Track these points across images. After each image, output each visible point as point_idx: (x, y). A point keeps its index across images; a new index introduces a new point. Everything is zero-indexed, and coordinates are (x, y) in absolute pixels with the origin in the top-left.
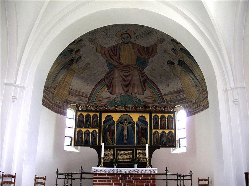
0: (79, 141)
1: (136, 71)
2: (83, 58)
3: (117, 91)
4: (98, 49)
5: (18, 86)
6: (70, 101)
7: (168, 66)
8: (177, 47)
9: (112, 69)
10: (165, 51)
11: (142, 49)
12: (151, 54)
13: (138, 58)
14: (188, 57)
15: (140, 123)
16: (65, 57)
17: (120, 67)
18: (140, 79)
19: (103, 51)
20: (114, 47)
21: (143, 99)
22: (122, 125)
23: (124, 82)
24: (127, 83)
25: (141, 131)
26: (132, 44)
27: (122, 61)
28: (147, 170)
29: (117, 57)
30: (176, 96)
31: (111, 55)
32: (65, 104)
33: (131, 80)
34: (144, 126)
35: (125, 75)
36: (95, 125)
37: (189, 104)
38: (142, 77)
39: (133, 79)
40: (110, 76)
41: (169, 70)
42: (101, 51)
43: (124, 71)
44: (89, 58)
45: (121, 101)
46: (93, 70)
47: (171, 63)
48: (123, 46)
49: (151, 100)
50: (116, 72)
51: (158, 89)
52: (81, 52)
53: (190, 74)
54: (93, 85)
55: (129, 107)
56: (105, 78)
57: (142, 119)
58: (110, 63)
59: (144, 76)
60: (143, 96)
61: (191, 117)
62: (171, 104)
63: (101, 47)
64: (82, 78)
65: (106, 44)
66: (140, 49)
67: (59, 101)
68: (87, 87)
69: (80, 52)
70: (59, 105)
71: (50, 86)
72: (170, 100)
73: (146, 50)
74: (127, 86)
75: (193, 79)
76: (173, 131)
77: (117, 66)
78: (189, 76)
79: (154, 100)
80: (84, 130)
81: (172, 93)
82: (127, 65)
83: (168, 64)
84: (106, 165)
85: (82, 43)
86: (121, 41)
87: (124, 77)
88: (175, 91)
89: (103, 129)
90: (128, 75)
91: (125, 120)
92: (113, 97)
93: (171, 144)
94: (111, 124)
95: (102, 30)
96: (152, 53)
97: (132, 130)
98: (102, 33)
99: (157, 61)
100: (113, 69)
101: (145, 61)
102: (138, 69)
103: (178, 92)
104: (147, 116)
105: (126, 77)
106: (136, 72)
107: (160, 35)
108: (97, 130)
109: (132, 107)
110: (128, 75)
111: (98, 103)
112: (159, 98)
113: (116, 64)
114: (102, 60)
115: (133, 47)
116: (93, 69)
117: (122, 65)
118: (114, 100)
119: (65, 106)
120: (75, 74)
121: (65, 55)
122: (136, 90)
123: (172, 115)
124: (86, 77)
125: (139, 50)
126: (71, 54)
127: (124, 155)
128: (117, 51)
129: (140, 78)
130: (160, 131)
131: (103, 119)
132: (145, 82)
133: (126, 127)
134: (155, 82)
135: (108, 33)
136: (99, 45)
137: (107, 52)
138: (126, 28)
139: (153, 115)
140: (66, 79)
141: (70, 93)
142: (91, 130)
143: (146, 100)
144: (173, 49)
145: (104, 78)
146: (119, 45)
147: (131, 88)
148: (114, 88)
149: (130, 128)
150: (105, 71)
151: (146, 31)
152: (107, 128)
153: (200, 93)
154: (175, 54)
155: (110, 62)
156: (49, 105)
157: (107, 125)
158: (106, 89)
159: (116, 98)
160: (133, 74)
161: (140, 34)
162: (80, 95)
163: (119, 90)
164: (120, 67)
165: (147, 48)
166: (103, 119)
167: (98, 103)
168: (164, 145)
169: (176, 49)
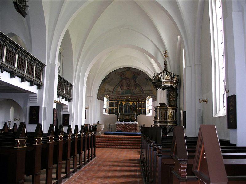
0: (110, 112)
5: (91, 96)
9: (122, 80)
20: (123, 72)
26: (130, 71)
27: (126, 76)
28: (135, 123)
45: (126, 92)
57: (133, 104)
61: (154, 102)
74: (128, 86)
76: (145, 108)
80: (112, 108)
81: (147, 91)
84: (120, 121)
93: (144, 113)
103: (150, 90)
104: (135, 103)
106: (133, 81)
108: (117, 108)
127: (127, 117)
130: (140, 108)
131: (119, 104)
132: (136, 85)
137: (120, 74)
139: (138, 102)
141: (105, 91)
142: (115, 108)
162: (108, 91)
163: (125, 88)
166: (119, 104)
168: (141, 114)
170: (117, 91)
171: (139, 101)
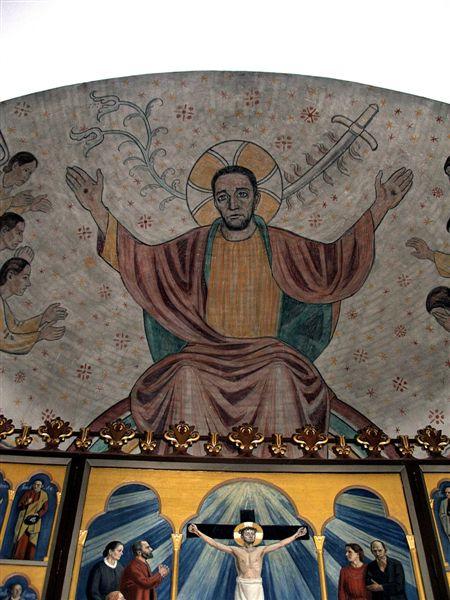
1: (279, 370)
2: (33, 271)
4: (107, 247)
7: (433, 319)
10: (414, 242)
11: (307, 255)
12: (350, 276)
13: (289, 305)
15: (347, 533)
19: (132, 262)
20: (181, 243)
22: (222, 545)
25: (367, 582)
26: (260, 227)
27: (214, 319)
29: (191, 301)
31: (165, 284)
33: (255, 417)
34: (382, 550)
35: (227, 390)
36: (30, 545)
38: (310, 398)
40: (158, 391)
42: (122, 258)
43: (226, 369)
44: (62, 282)
48: (220, 241)
50: (188, 374)
52: (32, 229)
56: (135, 400)
58: (158, 328)
59: (318, 392)
63: (126, 237)
64: (21, 376)
65: (145, 222)
66: (298, 258)
69: (20, 233)
73: (322, 257)
77: (194, 344)
82: (237, 342)
83: (429, 310)
87: (222, 401)
89: (82, 570)
90: (244, 393)
91: (247, 515)
94: (146, 537)
95: (129, 129)
96: (353, 268)
97: (300, 581)
100: (171, 359)
105: (233, 398)
106: (280, 377)
107: (390, 154)
110: (244, 393)
113: (188, 335)
114: (126, 307)
115: (267, 246)
116: (80, 341)
124: (43, 378)
125: (292, 261)
128: (192, 265)
129: (298, 402)
131: (93, 506)
133: (251, 559)
135: (158, 159)
136: (113, 226)
137: (147, 269)
145: (130, 397)
146: (202, 238)
149: (284, 568)
151: (328, 144)
152: (111, 563)
155: (161, 320)
157: (113, 546)
160: (266, 386)
161: (297, 169)
165: (330, 249)
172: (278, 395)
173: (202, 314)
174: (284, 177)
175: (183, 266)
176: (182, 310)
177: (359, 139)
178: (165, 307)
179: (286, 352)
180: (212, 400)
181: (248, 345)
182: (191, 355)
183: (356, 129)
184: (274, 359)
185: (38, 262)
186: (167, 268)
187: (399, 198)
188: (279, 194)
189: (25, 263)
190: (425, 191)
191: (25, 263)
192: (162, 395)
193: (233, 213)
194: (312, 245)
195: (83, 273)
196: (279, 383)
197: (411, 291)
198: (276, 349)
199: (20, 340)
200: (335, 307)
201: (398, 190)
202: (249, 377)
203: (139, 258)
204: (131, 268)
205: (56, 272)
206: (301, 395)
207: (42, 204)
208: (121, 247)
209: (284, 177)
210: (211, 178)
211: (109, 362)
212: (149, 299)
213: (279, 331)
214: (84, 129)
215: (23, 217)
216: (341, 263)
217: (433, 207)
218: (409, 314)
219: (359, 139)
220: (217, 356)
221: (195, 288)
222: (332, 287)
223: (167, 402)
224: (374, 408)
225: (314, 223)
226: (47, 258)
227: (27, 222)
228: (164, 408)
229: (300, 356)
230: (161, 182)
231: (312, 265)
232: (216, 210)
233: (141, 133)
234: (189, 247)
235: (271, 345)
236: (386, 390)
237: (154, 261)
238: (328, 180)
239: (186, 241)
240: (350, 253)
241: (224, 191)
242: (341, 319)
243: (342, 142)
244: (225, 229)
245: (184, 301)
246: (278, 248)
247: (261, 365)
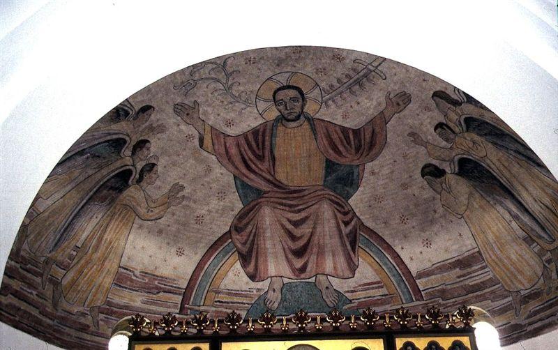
1: (326, 206)
2: (160, 169)
3: (272, 270)
4: (205, 142)
6: (121, 307)
8: (454, 117)
9: (252, 198)
10: (412, 134)
11: (341, 135)
13: (330, 166)
14: (495, 144)
16: (99, 161)
17: (277, 195)
18: (340, 231)
19: (223, 148)
20: (255, 132)
21: (352, 292)
23: (290, 243)
24: (301, 243)
26: (310, 120)
27: (281, 176)
29: (267, 165)
30: (459, 277)
31: (247, 158)
32: (102, 316)
33: (311, 236)
37: (507, 300)
38: (346, 224)
39: (318, 230)
41: (428, 193)
42: (216, 147)
43: (290, 206)
44: (179, 169)
45: (283, 300)
46: (192, 204)
47: (433, 172)
48: (281, 128)
49: (376, 293)
51: (397, 257)
52: (155, 145)
53: (503, 200)
54: (196, 254)
55: (314, 319)
56: (234, 232)
59: (351, 220)
60: (352, 283)
62: (444, 302)
64: (160, 232)
65: (229, 123)
66: (335, 137)
67: (81, 309)
68: (176, 260)
69: (148, 149)
70: (82, 320)
71: (43, 259)
72: (438, 291)
73: (351, 137)
74: (299, 253)
75: (516, 218)
78: (499, 208)
79: (387, 293)
83: (423, 176)
85: (153, 117)
86: (274, 114)
87: (290, 227)
88: (453, 260)
92: (258, 290)
95: (213, 76)
96: (372, 145)
98: (213, 85)
99: (389, 171)
101: (351, 173)
102: (330, 200)
105: (297, 224)
106: (326, 211)
109: (323, 320)
111: (214, 309)
112: (403, 286)
113: (264, 186)
114: (222, 175)
115: (313, 129)
117: (284, 189)
118: (263, 299)
119: (101, 322)
120: (138, 221)
121: (99, 157)
122: (329, 265)
123: (465, 340)
125: (331, 139)
126: (119, 152)
129: (338, 226)
134: (385, 238)
136: (208, 129)
137: (234, 151)
138: (288, 70)
139: (400, 342)
140: (108, 236)
143: (361, 294)
144: (440, 126)
145: (230, 231)
146: (269, 127)
147: (313, 258)
148: (261, 260)
150: (233, 210)
151: (352, 73)
153: (549, 261)
154: (447, 140)
156: (39, 322)
158: (238, 265)
159: (271, 292)
163: (277, 267)
164: (277, 195)
165: (356, 132)
167: (214, 309)
169: (451, 125)
170: (217, 292)
171: (405, 331)
172: (325, 222)
173: (273, 173)
174: (322, 91)
175: (258, 145)
176: (260, 172)
177: (373, 73)
178: (248, 172)
179: (330, 195)
180: (283, 226)
181: (305, 190)
182: (268, 199)
183: (370, 67)
184: (321, 199)
185: (162, 163)
186: (246, 148)
187: (402, 107)
188: (320, 100)
189: (154, 165)
190: (419, 107)
191: (154, 165)
192: (250, 227)
193: (289, 112)
194: (344, 130)
195: (192, 161)
196: (326, 214)
197: (411, 163)
198: (323, 192)
199: (156, 211)
200: (361, 168)
201: (401, 103)
202: (305, 211)
203: (227, 145)
204: (223, 151)
205: (174, 164)
206: (340, 222)
207: (162, 128)
208: (216, 141)
209: (322, 91)
210: (272, 93)
211: (214, 210)
212: (237, 168)
213: (325, 181)
214: (182, 83)
215: (149, 139)
216: (366, 141)
217: (426, 117)
218: (411, 177)
219: (373, 73)
220: (285, 198)
221: (267, 158)
222: (358, 156)
223: (254, 231)
224: (387, 233)
225: (345, 117)
226: (167, 158)
227: (152, 141)
228: (252, 234)
229: (338, 197)
230: (239, 99)
231: (345, 141)
232: (278, 112)
233: (221, 76)
234: (260, 134)
235: (320, 190)
236: (395, 222)
237: (238, 145)
238: (352, 93)
239: (258, 130)
240: (370, 135)
241: (282, 100)
242: (365, 175)
243: (361, 74)
244: (284, 121)
245: (260, 166)
246: (321, 131)
247: (314, 202)
